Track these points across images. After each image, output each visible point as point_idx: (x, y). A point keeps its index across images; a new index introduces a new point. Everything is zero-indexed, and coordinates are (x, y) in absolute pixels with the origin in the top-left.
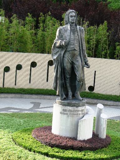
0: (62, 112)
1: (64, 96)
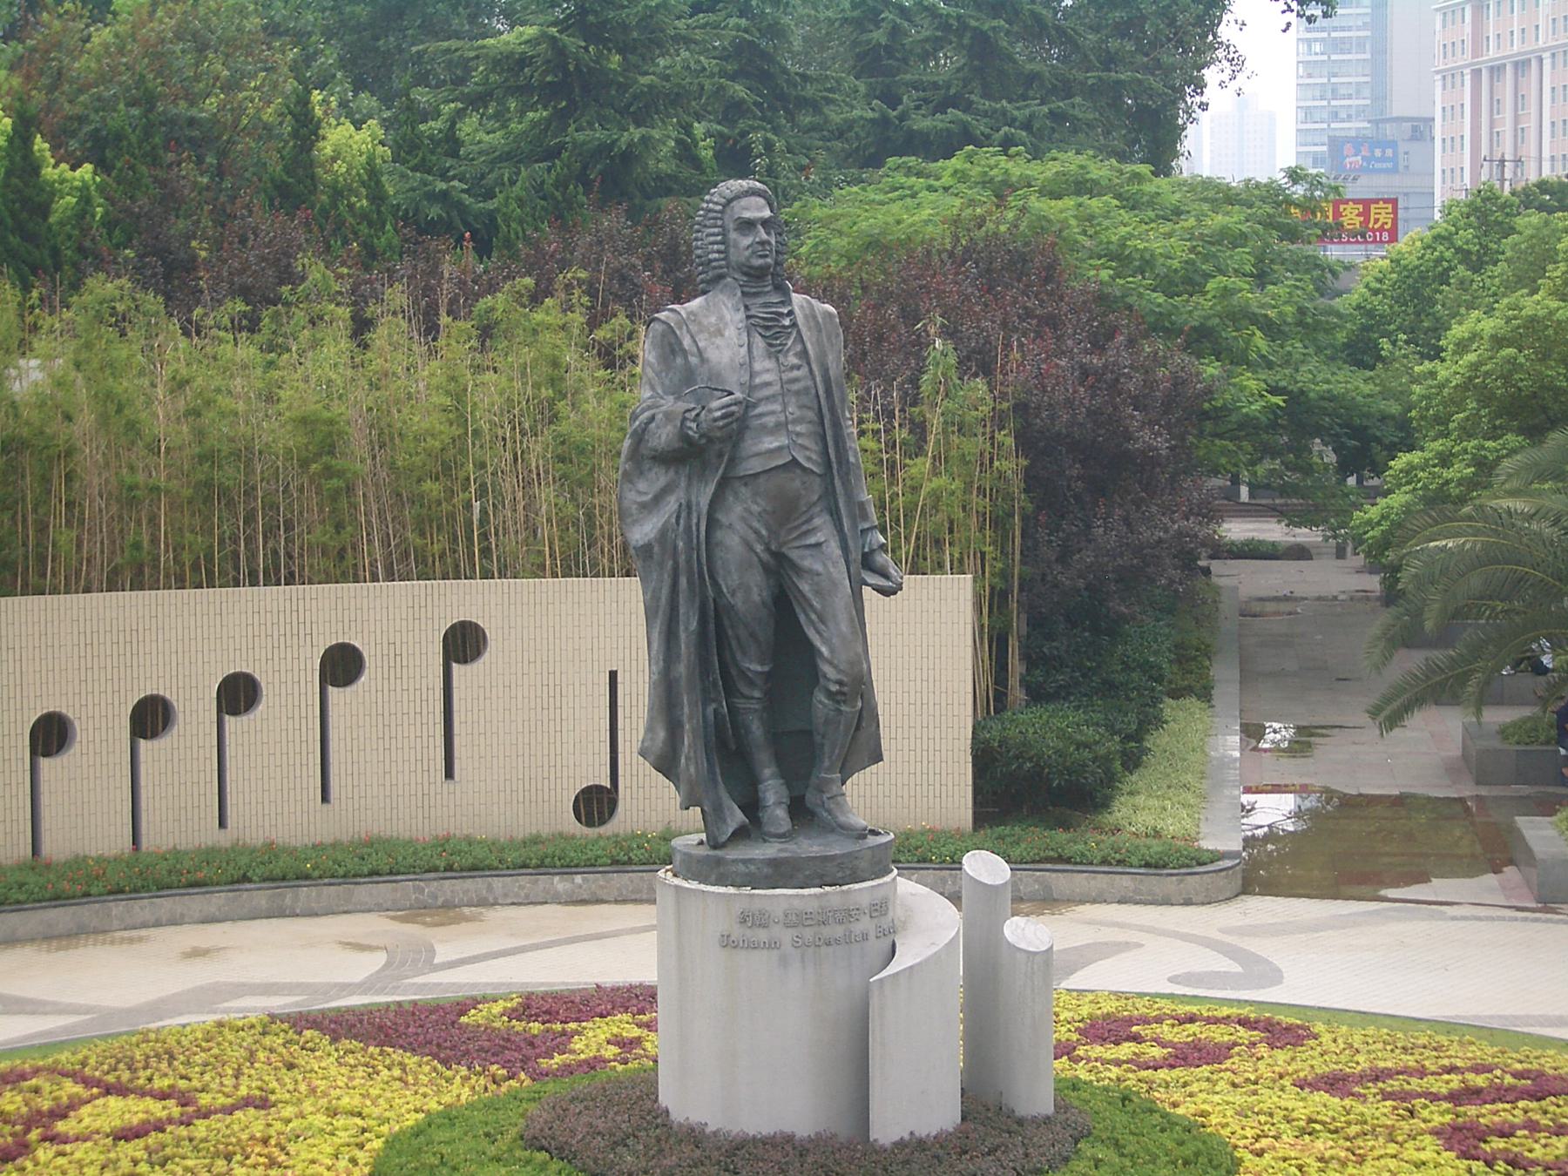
0: (737, 932)
1: (736, 817)
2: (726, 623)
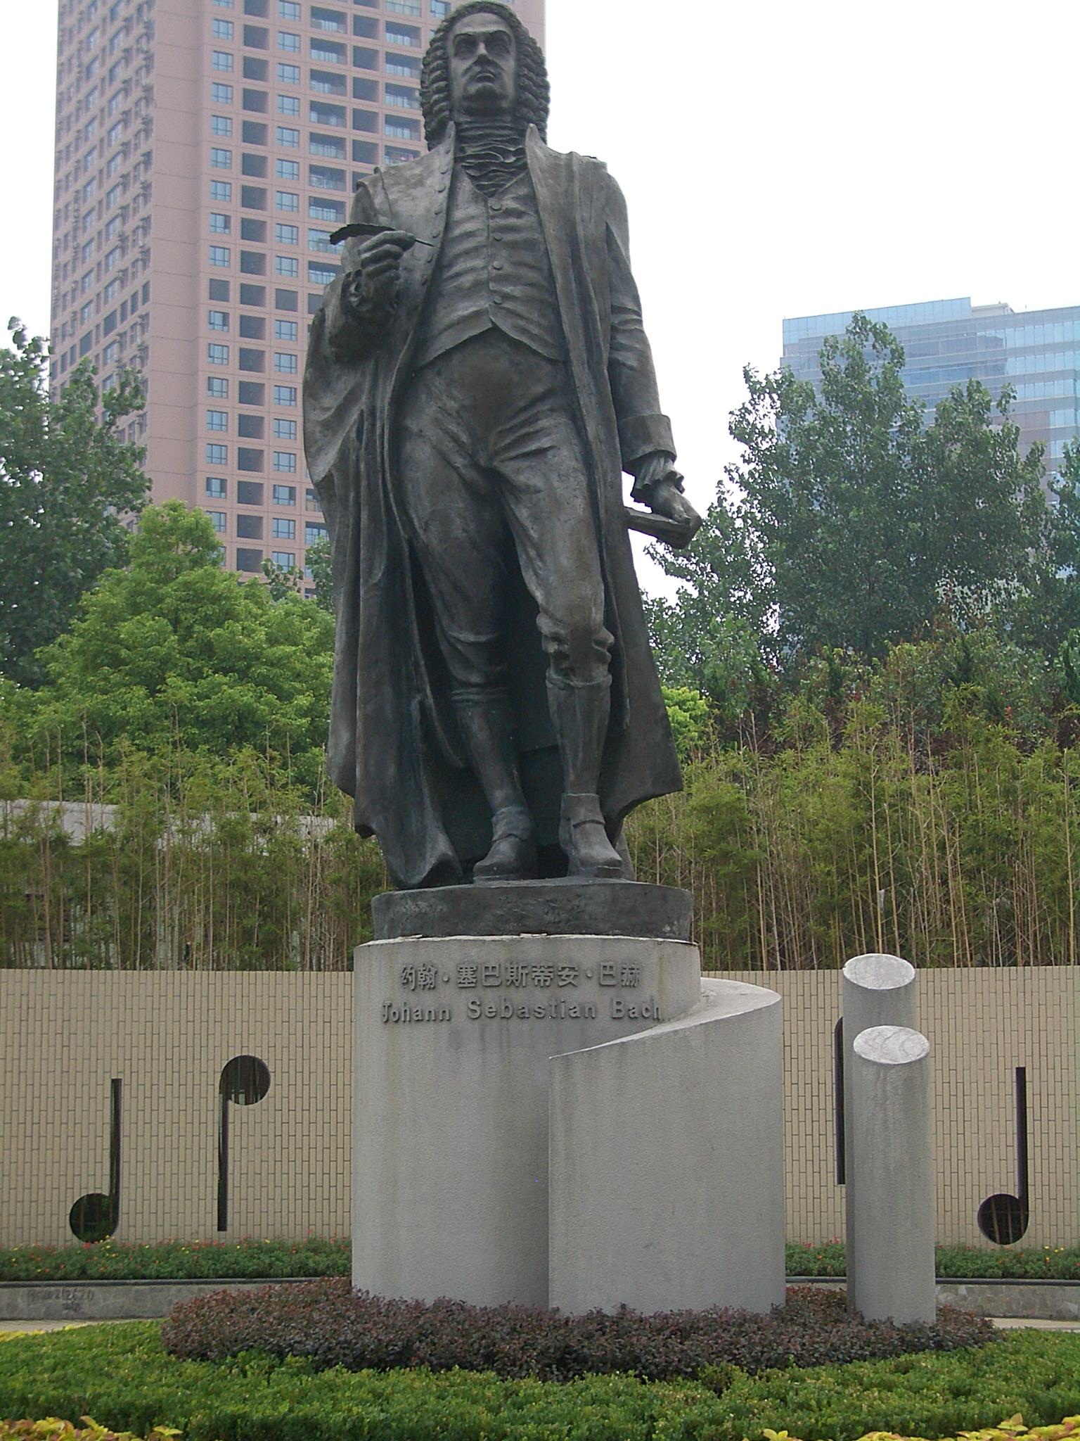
0: (400, 998)
2: (428, 577)
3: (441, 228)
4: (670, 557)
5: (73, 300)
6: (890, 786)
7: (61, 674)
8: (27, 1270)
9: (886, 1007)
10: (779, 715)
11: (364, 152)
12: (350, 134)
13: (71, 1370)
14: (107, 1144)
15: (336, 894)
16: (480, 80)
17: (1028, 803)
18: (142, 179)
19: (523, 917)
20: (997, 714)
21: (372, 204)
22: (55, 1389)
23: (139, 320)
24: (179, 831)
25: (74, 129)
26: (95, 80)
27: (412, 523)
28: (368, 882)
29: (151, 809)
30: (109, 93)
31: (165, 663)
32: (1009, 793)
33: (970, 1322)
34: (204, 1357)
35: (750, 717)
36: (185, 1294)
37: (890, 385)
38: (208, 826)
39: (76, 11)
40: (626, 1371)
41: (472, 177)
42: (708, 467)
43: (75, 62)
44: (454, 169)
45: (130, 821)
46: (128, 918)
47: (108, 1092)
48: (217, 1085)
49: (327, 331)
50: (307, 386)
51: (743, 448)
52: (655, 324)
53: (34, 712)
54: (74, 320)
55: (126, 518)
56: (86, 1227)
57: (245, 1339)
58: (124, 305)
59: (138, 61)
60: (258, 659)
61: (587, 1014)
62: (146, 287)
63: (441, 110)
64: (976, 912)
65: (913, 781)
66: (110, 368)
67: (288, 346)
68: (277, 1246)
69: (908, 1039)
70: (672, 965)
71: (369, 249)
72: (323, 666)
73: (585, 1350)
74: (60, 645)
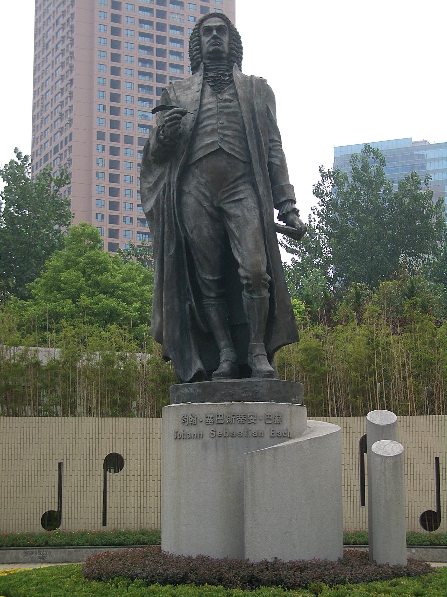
0: (182, 429)
2: (193, 252)
3: (198, 107)
4: (288, 245)
5: (41, 140)
6: (382, 340)
7: (36, 295)
8: (23, 542)
9: (385, 432)
10: (336, 310)
11: (161, 79)
12: (155, 71)
13: (44, 585)
14: (57, 490)
15: (151, 385)
16: (214, 45)
17: (439, 347)
18: (69, 90)
19: (233, 395)
20: (426, 310)
21: (169, 97)
22: (38, 593)
23: (68, 148)
24: (86, 359)
25: (41, 70)
26: (50, 49)
27: (186, 230)
28: (165, 380)
29: (75, 350)
30: (56, 55)
31: (80, 290)
32: (431, 343)
33: (422, 565)
34: (100, 580)
35: (324, 312)
36: (86, 553)
37: (379, 173)
38: (98, 357)
39: (42, 21)
40: (277, 586)
41: (211, 86)
42: (307, 206)
43: (41, 42)
44: (203, 82)
45: (66, 355)
46: (65, 395)
47: (57, 468)
48: (102, 465)
49: (150, 150)
50: (142, 173)
51: (318, 200)
52: (286, 147)
53: (25, 310)
54: (41, 148)
55: (64, 229)
56: (48, 524)
57: (117, 572)
58: (62, 142)
59: (67, 41)
60: (118, 288)
61: (260, 435)
62: (71, 134)
63: (198, 58)
64: (418, 392)
65: (392, 338)
66: (56, 168)
67: (132, 159)
68: (127, 532)
69: (394, 446)
70: (295, 414)
71: (170, 115)
72: (145, 290)
73: (260, 577)
74: (36, 282)
